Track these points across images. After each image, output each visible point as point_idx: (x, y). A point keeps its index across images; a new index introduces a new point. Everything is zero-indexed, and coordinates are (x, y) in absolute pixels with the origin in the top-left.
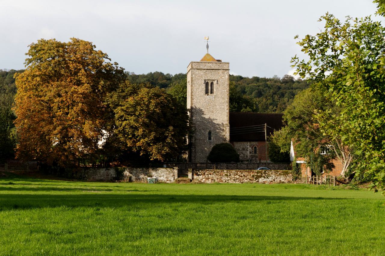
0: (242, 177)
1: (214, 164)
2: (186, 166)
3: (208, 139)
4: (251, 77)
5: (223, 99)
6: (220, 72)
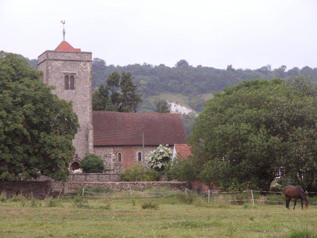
4: (75, 47)
6: (82, 64)
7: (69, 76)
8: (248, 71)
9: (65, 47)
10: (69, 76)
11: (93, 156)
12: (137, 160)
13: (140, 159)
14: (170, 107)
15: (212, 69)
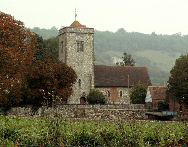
0: (122, 114)
1: (91, 105)
2: (70, 106)
3: (78, 86)
4: (83, 24)
5: (90, 55)
6: (88, 35)
7: (80, 43)
8: (107, 32)
9: (76, 24)
10: (80, 43)
11: (94, 92)
12: (120, 96)
13: (121, 95)
14: (113, 60)
15: (141, 34)
